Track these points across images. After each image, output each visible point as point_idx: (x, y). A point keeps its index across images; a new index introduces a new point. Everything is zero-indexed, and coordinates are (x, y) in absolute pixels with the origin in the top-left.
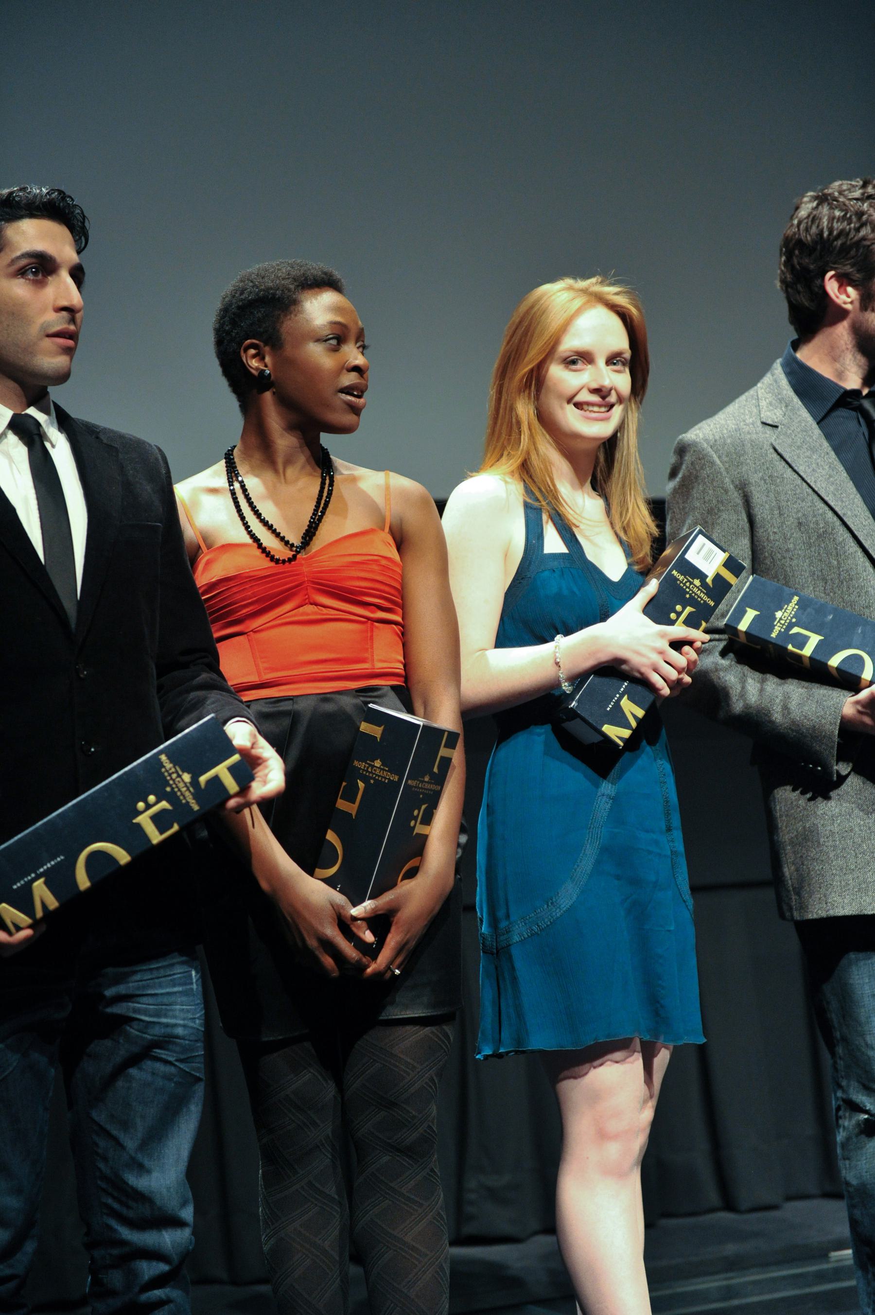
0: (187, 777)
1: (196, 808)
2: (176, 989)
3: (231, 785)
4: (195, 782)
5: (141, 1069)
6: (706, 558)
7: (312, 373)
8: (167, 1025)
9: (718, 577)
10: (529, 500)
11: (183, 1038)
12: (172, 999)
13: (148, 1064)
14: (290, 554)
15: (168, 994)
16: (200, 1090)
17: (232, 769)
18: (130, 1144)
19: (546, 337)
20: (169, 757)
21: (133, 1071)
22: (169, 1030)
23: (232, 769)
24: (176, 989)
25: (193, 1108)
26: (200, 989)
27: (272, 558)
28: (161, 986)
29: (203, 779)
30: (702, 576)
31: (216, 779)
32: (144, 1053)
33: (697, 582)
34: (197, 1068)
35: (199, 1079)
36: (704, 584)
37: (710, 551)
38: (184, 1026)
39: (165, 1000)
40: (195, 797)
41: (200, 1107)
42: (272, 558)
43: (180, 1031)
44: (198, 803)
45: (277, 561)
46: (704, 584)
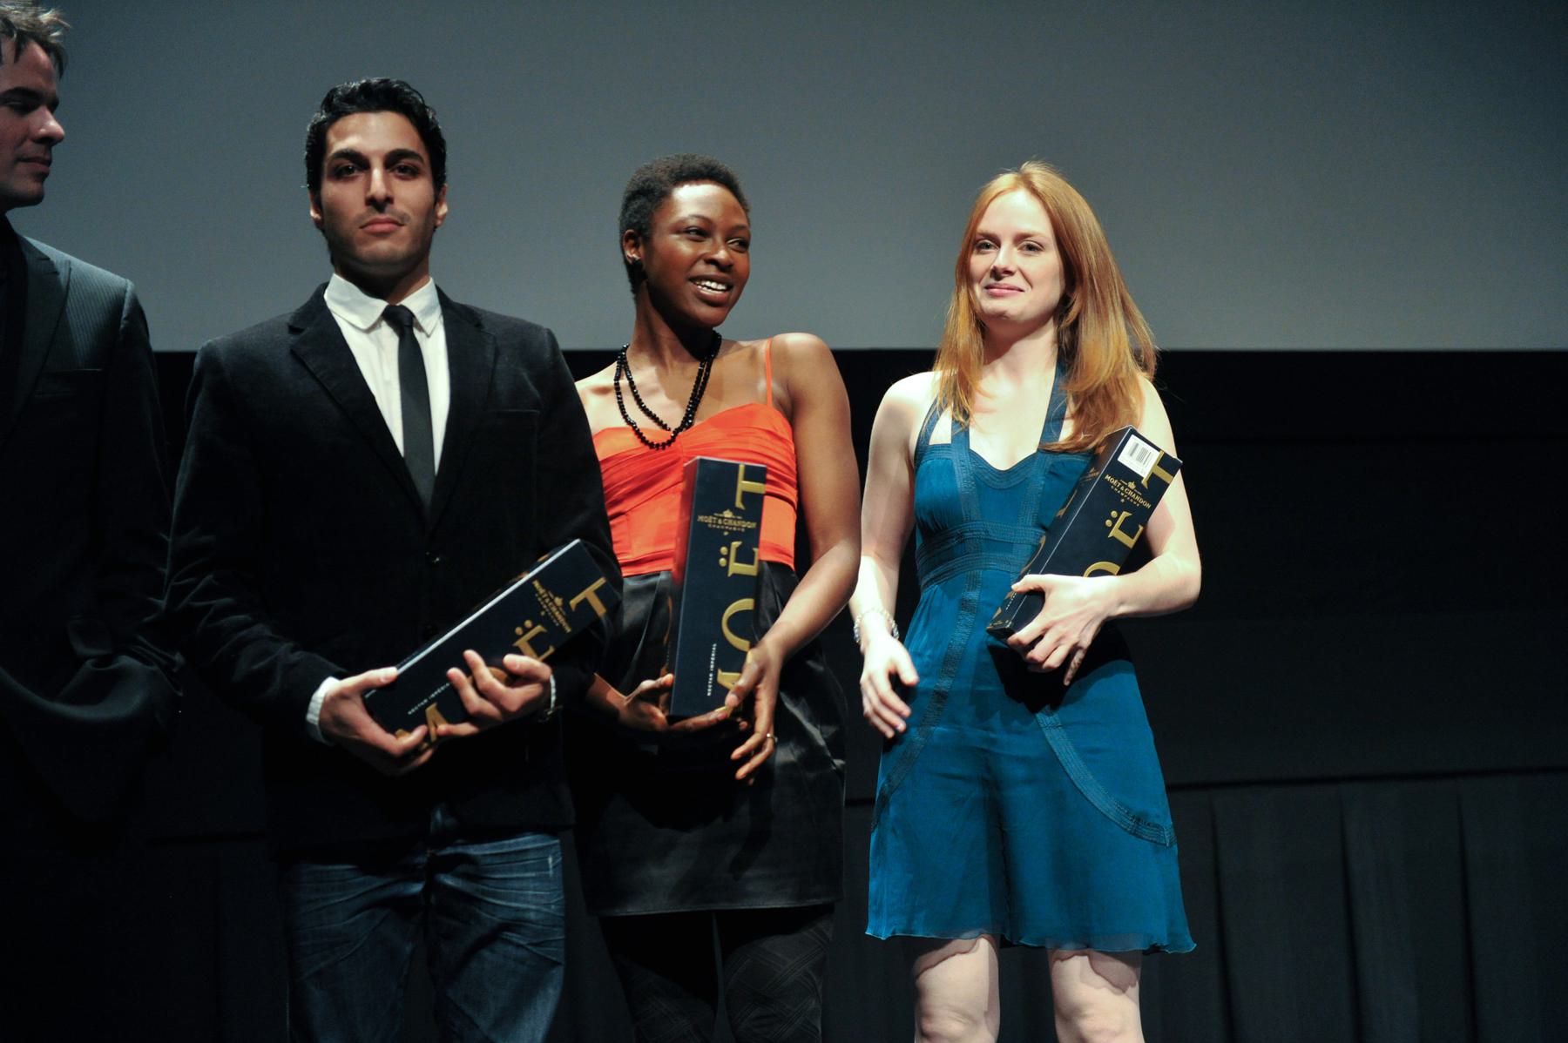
0: (558, 601)
1: (568, 630)
2: (528, 875)
3: (600, 609)
4: (566, 605)
5: (493, 951)
6: (1140, 459)
7: (672, 259)
8: (518, 909)
9: (1153, 477)
10: (197, 360)
11: (536, 923)
12: (525, 884)
13: (500, 947)
14: (668, 435)
15: (518, 879)
16: (558, 974)
17: (598, 592)
18: (484, 1023)
19: (667, 354)
20: (543, 585)
21: (486, 953)
22: (519, 915)
23: (598, 592)
24: (528, 875)
25: (551, 991)
26: (559, 875)
27: (643, 440)
28: (511, 871)
29: (573, 602)
30: (1136, 478)
31: (585, 602)
32: (494, 936)
33: (1132, 485)
34: (556, 952)
35: (556, 964)
36: (1139, 486)
37: (1144, 451)
38: (537, 911)
39: (516, 884)
40: (567, 619)
41: (559, 990)
42: (643, 440)
43: (532, 916)
44: (570, 625)
45: (651, 445)
46: (1139, 486)
